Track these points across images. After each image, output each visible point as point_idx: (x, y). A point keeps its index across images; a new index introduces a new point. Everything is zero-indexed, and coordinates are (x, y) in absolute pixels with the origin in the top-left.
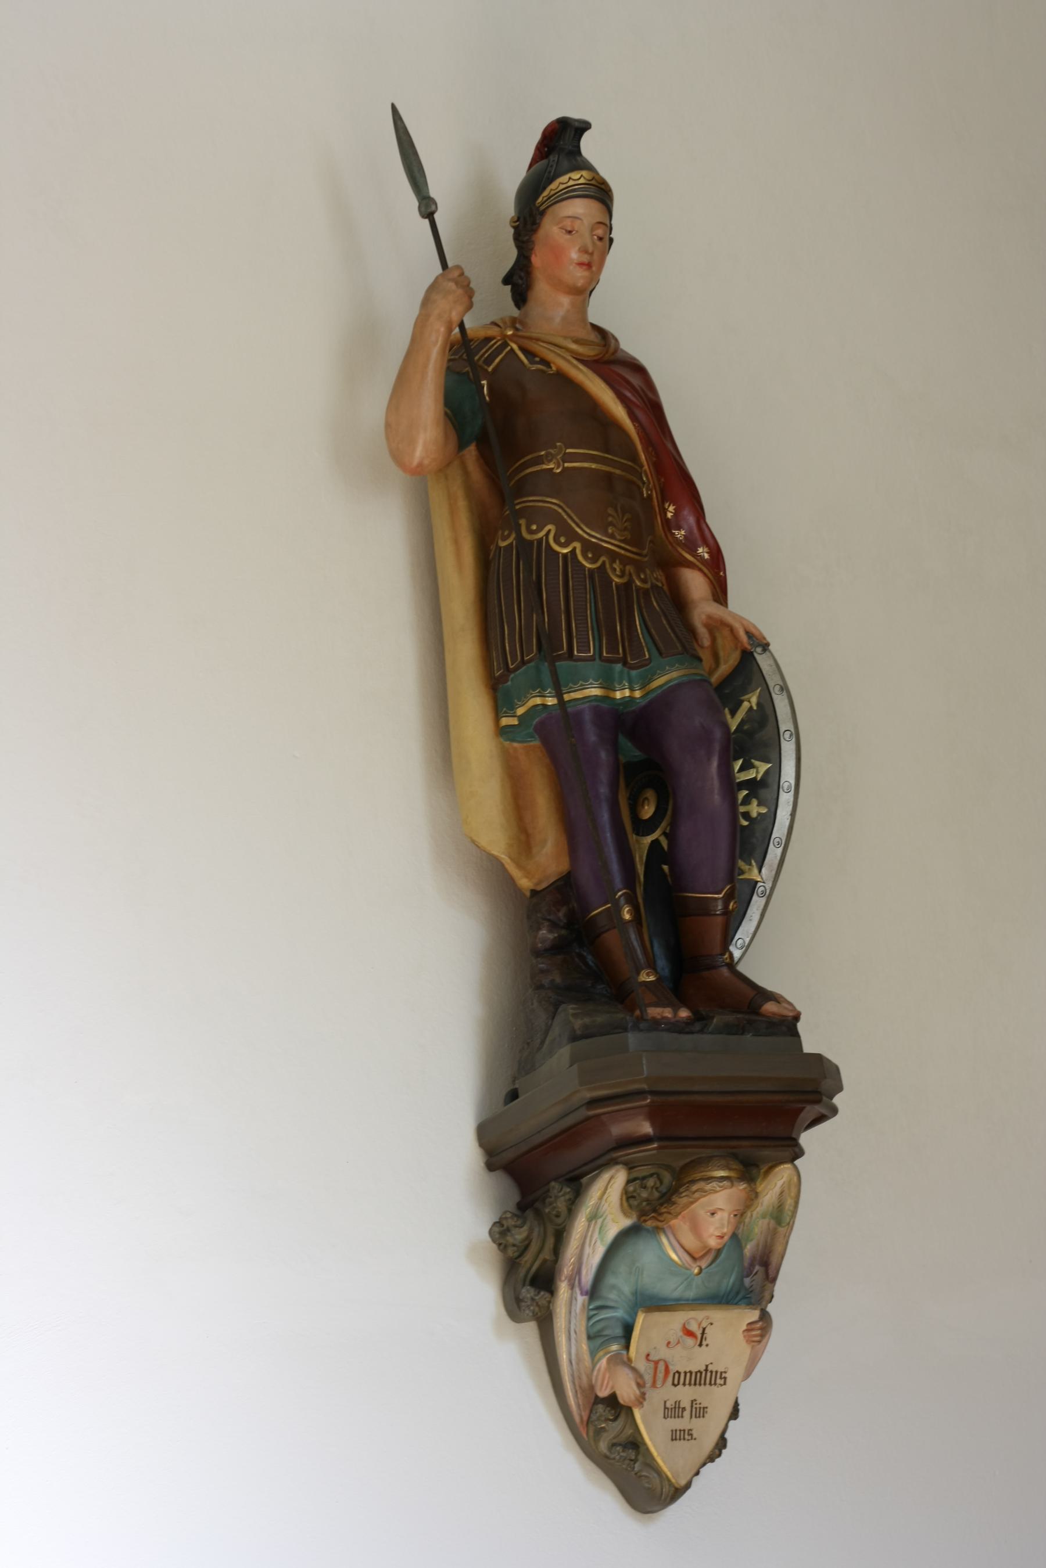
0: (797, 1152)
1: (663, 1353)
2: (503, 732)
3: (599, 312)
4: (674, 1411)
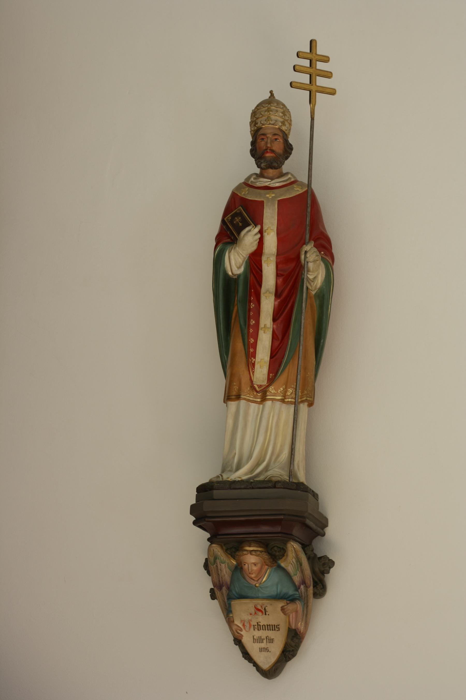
4: (260, 640)
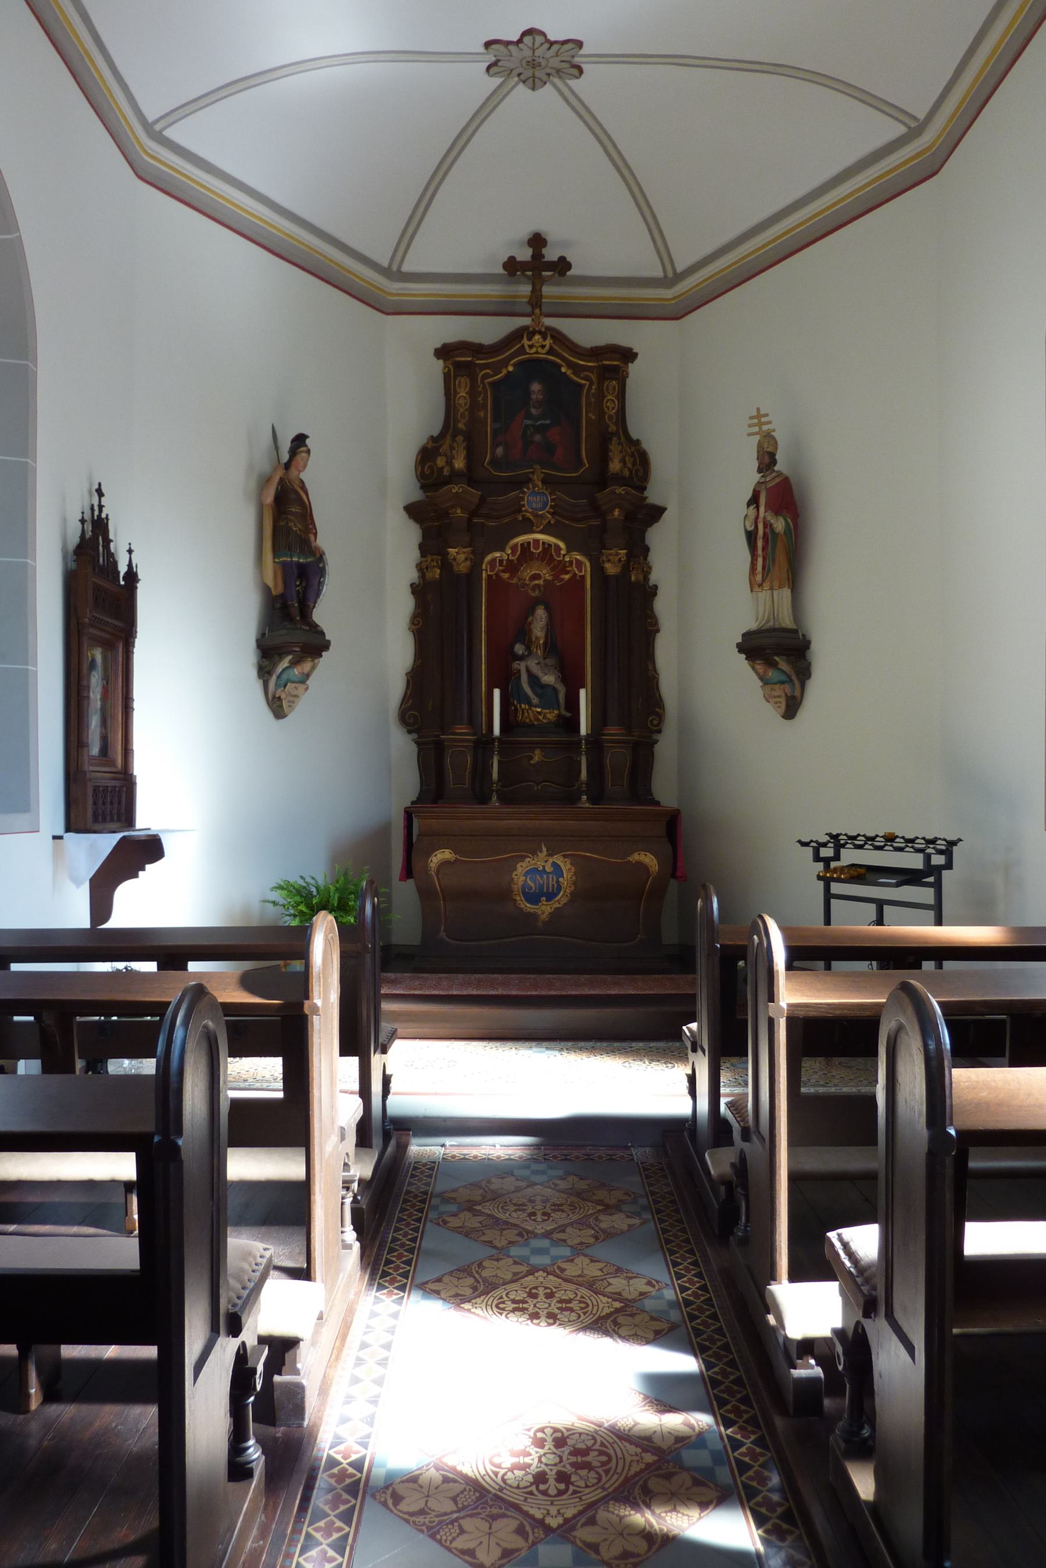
0: (321, 656)
1: (291, 691)
2: (274, 562)
3: (302, 476)
4: (289, 702)
